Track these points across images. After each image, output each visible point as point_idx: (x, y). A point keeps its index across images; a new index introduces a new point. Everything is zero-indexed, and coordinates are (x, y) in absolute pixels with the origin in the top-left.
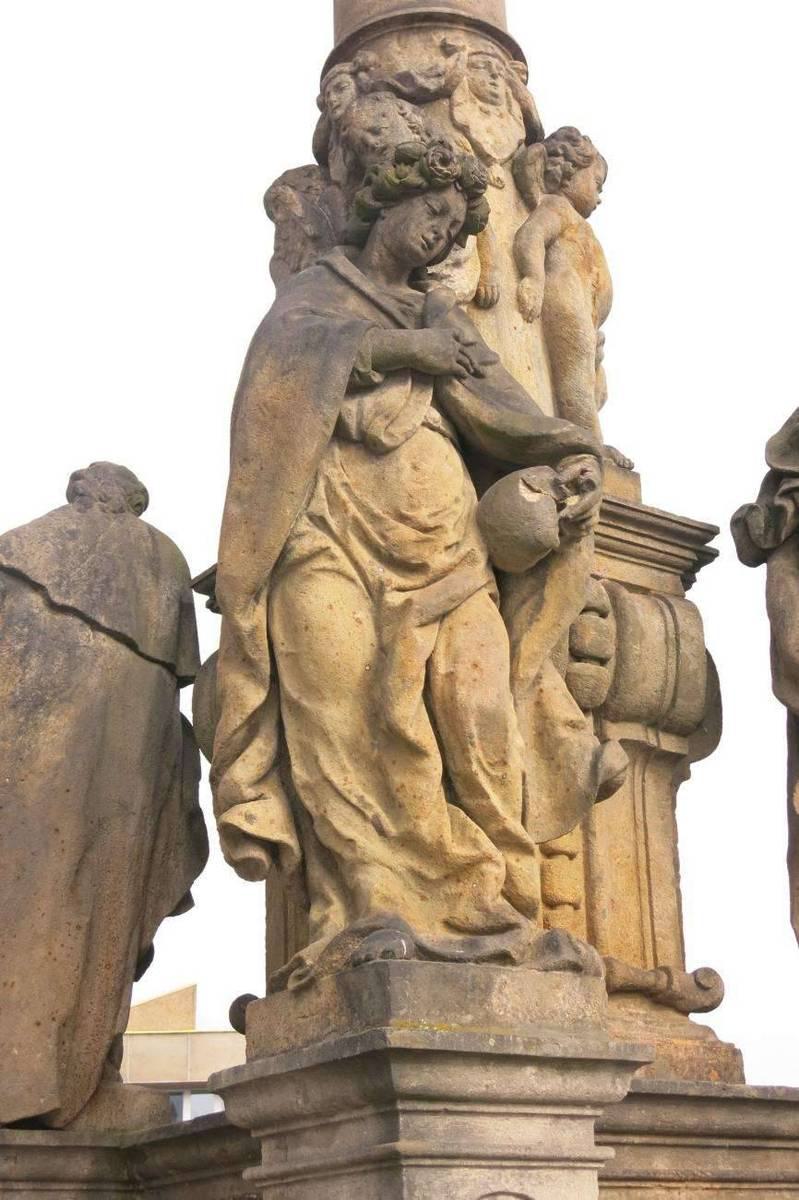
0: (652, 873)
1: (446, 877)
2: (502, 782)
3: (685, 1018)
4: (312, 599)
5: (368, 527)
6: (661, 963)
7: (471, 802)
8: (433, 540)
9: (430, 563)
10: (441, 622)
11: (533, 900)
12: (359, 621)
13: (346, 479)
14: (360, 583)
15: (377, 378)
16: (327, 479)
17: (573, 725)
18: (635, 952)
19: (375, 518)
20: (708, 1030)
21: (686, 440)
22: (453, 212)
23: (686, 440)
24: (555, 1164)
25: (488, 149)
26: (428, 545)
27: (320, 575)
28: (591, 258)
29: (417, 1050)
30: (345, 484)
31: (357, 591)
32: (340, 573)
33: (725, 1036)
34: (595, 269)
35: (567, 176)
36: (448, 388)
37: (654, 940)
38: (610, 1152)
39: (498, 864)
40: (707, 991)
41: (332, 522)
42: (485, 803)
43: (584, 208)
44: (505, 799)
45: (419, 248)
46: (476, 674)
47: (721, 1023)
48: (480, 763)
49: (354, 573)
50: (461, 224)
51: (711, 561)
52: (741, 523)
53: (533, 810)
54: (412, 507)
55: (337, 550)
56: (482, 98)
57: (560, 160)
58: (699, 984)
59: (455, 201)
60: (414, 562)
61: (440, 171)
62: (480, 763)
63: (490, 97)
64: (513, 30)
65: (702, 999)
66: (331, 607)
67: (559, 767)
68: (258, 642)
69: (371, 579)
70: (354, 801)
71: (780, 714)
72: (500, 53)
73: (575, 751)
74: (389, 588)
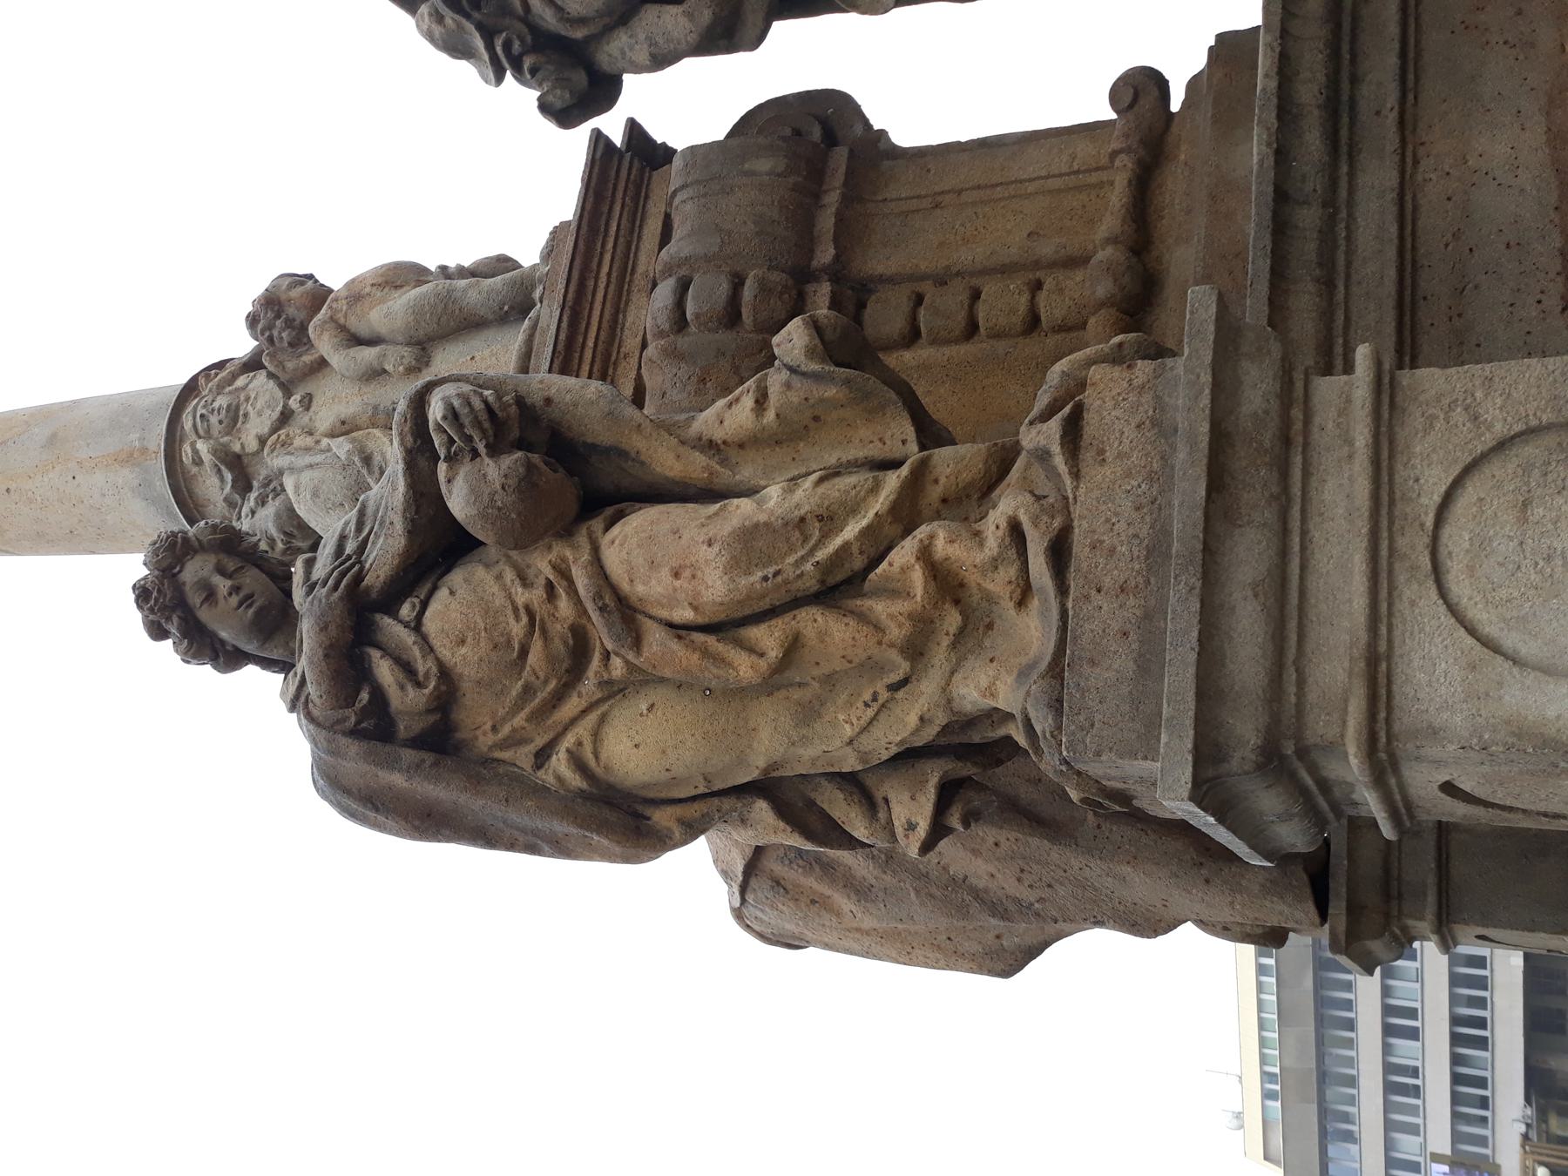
0: (993, 181)
1: (957, 602)
2: (829, 520)
3: (1176, 120)
4: (632, 764)
5: (541, 696)
6: (1104, 161)
7: (858, 563)
8: (542, 620)
9: (569, 622)
10: (635, 610)
11: (990, 455)
12: (651, 708)
13: (488, 726)
14: (604, 708)
15: (365, 696)
16: (490, 748)
17: (761, 401)
18: (1093, 197)
19: (528, 691)
20: (1193, 85)
21: (492, 177)
22: (205, 573)
23: (492, 177)
24: (1384, 607)
25: (276, 415)
26: (549, 624)
27: (603, 756)
28: (357, 293)
29: (1211, 443)
30: (494, 729)
31: (616, 712)
32: (596, 735)
33: (1199, 62)
34: (368, 290)
35: (289, 323)
36: (374, 595)
37: (1078, 172)
38: (1362, 353)
39: (932, 537)
40: (1139, 88)
41: (540, 741)
42: (855, 549)
43: (320, 295)
44: (853, 510)
45: (251, 611)
46: (687, 573)
47: (1181, 66)
48: (803, 559)
49: (593, 717)
50: (222, 556)
51: (639, 126)
52: (564, 114)
53: (875, 451)
54: (509, 642)
55: (568, 741)
56: (235, 420)
57: (275, 333)
58: (1131, 106)
59: (195, 570)
60: (571, 642)
61: (156, 600)
62: (803, 559)
63: (231, 414)
64: (183, 379)
65: (1148, 102)
66: (636, 746)
67: (816, 419)
68: (697, 815)
69: (599, 695)
70: (870, 713)
71: (781, 29)
72: (190, 409)
73: (795, 398)
74: (606, 677)
